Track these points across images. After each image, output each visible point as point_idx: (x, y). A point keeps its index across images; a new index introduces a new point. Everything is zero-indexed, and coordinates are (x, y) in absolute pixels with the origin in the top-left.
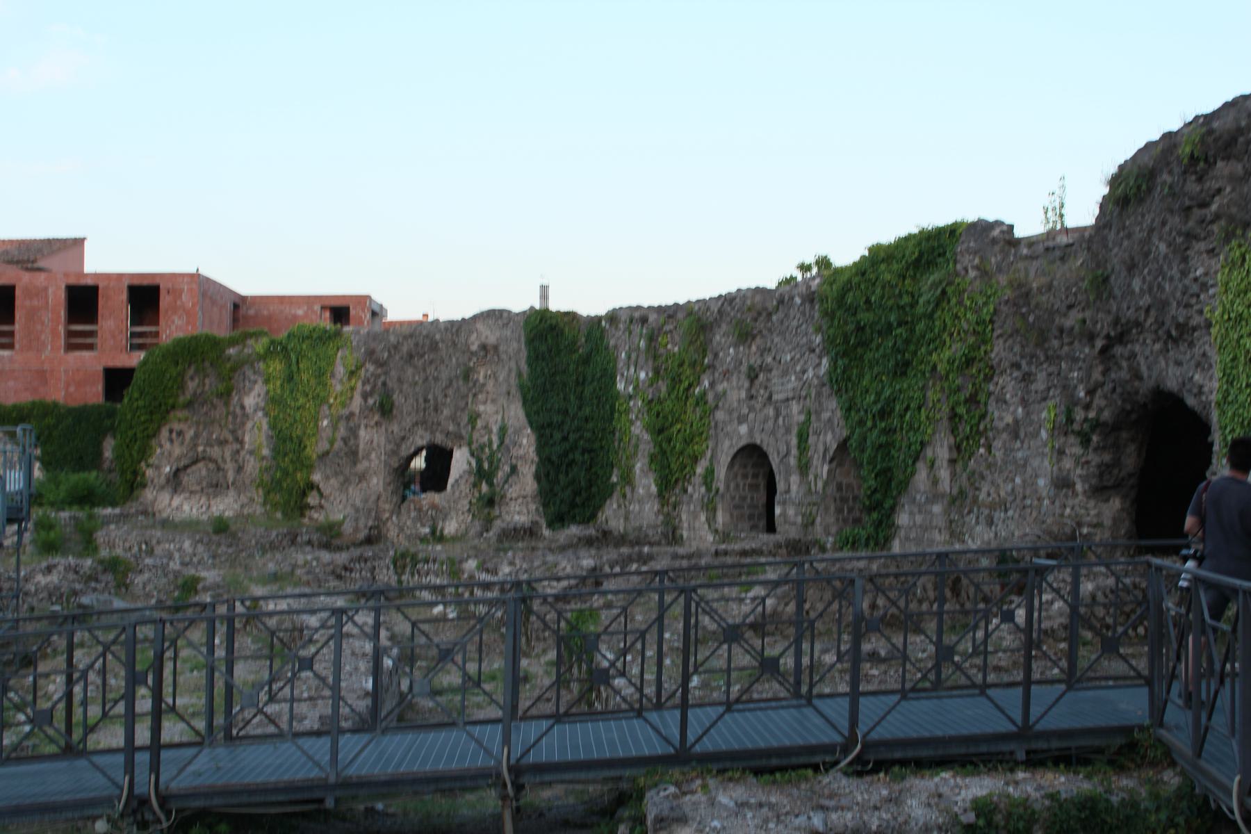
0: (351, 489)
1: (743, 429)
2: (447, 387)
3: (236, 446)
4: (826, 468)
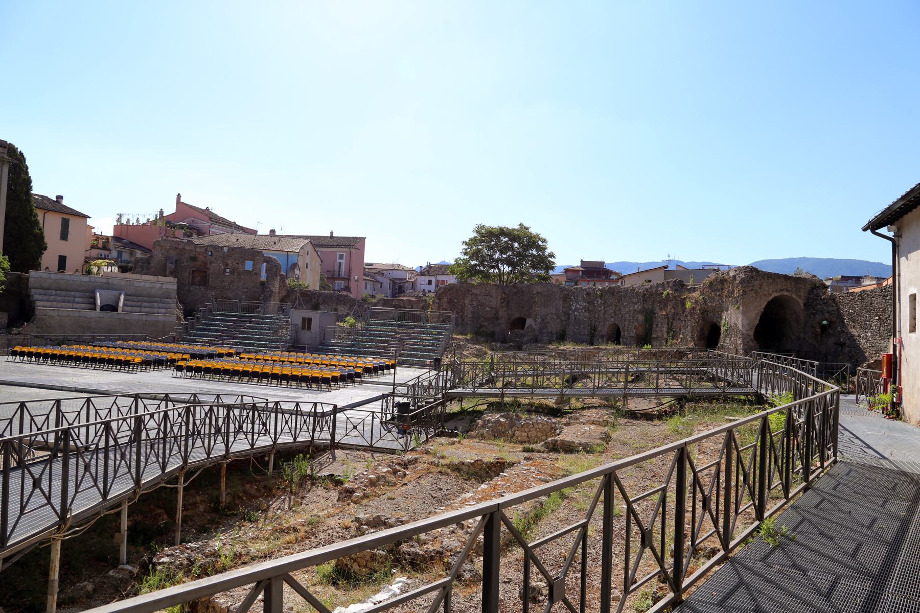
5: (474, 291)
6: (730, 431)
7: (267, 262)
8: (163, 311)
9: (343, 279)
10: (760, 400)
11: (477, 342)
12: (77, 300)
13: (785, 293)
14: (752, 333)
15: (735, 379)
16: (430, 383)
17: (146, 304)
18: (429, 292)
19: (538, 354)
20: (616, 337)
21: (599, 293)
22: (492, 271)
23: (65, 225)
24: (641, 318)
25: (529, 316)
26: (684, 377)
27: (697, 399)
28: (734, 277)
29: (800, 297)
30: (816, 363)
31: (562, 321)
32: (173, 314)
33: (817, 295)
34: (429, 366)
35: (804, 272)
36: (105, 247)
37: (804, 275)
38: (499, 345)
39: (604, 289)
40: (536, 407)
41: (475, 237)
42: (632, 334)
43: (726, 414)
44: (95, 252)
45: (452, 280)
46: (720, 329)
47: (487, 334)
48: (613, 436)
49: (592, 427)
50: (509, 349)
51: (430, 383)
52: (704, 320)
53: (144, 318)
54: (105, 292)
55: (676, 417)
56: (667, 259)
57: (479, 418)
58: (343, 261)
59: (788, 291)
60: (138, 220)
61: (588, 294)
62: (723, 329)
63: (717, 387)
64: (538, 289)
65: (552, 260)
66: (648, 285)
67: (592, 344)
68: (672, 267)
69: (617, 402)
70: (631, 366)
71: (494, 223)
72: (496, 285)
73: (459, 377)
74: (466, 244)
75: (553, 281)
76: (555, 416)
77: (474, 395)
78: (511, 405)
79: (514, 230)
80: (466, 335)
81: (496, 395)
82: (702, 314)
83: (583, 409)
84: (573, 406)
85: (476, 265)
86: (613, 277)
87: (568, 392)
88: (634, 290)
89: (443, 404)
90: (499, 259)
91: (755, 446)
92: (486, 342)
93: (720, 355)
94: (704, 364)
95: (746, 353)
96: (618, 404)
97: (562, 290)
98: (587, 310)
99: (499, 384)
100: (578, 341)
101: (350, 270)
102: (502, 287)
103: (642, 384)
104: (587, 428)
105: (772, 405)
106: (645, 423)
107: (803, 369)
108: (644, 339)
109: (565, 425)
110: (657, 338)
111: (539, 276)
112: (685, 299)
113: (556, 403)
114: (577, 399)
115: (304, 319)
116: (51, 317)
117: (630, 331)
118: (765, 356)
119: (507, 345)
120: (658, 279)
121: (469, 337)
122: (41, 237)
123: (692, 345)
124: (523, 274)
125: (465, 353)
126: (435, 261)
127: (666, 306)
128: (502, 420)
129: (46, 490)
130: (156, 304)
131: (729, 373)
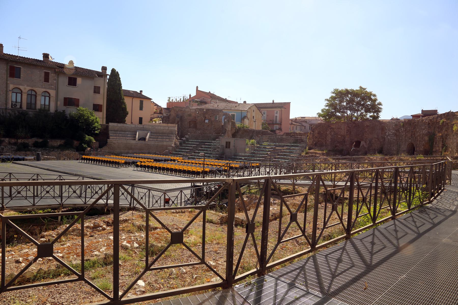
8: (168, 140)
9: (278, 124)
12: (128, 135)
17: (160, 137)
21: (402, 124)
23: (141, 103)
24: (427, 138)
32: (174, 141)
36: (160, 113)
42: (421, 149)
44: (156, 115)
53: (157, 143)
54: (141, 132)
58: (278, 115)
60: (176, 100)
65: (381, 106)
71: (342, 87)
79: (357, 90)
98: (395, 135)
101: (281, 119)
110: (436, 151)
115: (227, 142)
116: (115, 143)
122: (125, 109)
127: (442, 130)
129: (340, 213)
130: (165, 137)
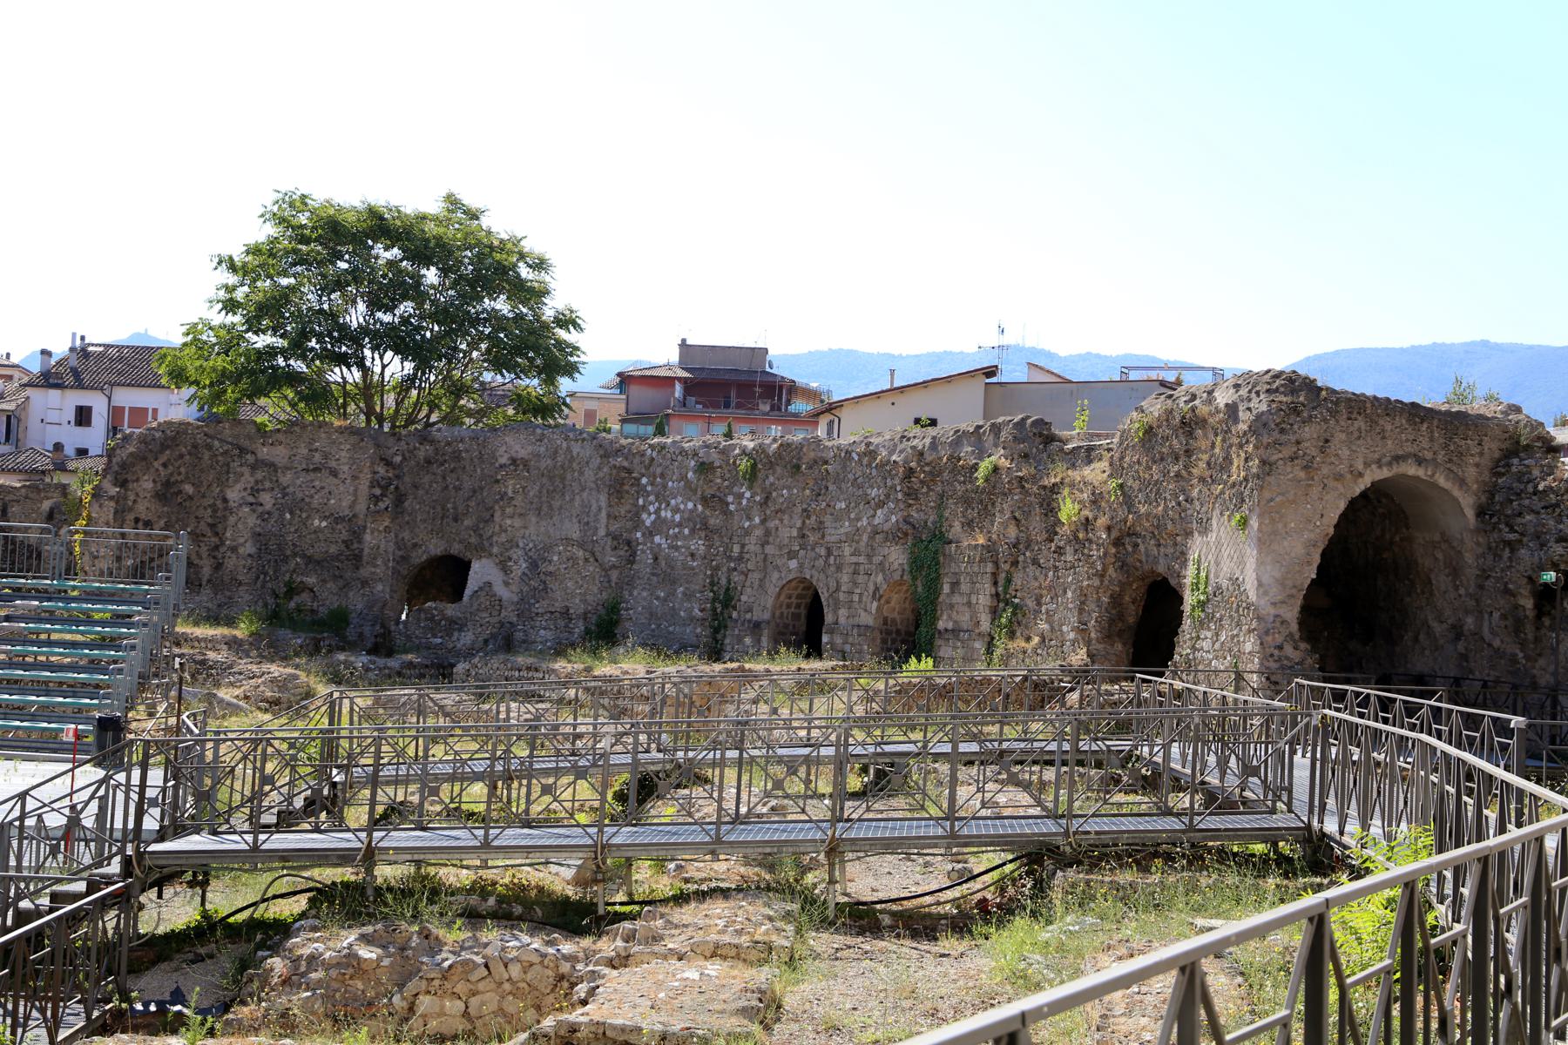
0: (351, 594)
1: (793, 564)
2: (469, 499)
3: (215, 540)
4: (875, 604)
5: (264, 452)
6: (1189, 971)
7: (349, 643)
10: (1320, 858)
11: (277, 652)
13: (1411, 470)
14: (1292, 613)
15: (1232, 781)
16: (74, 820)
18: (82, 452)
19: (515, 696)
20: (806, 628)
21: (744, 464)
22: (336, 375)
24: (897, 556)
25: (482, 550)
26: (1050, 774)
27: (1094, 854)
28: (1232, 409)
29: (1462, 482)
30: (1517, 721)
31: (606, 570)
33: (1524, 477)
34: (75, 748)
35: (1480, 392)
37: (1476, 407)
38: (360, 661)
39: (761, 449)
40: (501, 900)
41: (273, 241)
42: (866, 619)
43: (1199, 910)
45: (174, 407)
46: (1180, 600)
47: (308, 616)
48: (789, 1002)
49: (714, 968)
50: (401, 676)
51: (74, 820)
52: (1123, 566)
55: (1021, 922)
56: (994, 340)
57: (275, 950)
59: (1420, 461)
61: (704, 468)
62: (1189, 600)
63: (1168, 812)
64: (516, 445)
66: (922, 439)
67: (715, 654)
68: (1012, 373)
69: (804, 870)
70: (859, 735)
71: (348, 188)
72: (352, 431)
73: (195, 786)
74: (233, 267)
75: (576, 419)
76: (576, 931)
77: (254, 858)
78: (404, 893)
80: (231, 622)
81: (342, 857)
82: (1117, 543)
83: (681, 899)
84: (640, 892)
85: (271, 352)
86: (800, 406)
87: (623, 835)
88: (871, 453)
89: (125, 901)
90: (364, 330)
91: (1285, 1024)
92: (314, 650)
93: (1178, 695)
94: (1122, 728)
95: (1273, 685)
96: (810, 878)
97: (608, 452)
99: (357, 815)
100: (663, 644)
102: (377, 439)
103: (900, 802)
104: (693, 974)
105: (1357, 873)
106: (906, 948)
107: (1470, 745)
108: (908, 636)
109: (611, 964)
110: (956, 632)
111: (521, 401)
112: (1055, 489)
113: (578, 881)
114: (660, 864)
117: (856, 609)
118: (1339, 696)
119: (393, 663)
120: (962, 413)
121: (242, 631)
123: (1078, 657)
124: (458, 390)
125: (225, 694)
126: (107, 331)
127: (987, 512)
128: (367, 953)
131: (1212, 760)
